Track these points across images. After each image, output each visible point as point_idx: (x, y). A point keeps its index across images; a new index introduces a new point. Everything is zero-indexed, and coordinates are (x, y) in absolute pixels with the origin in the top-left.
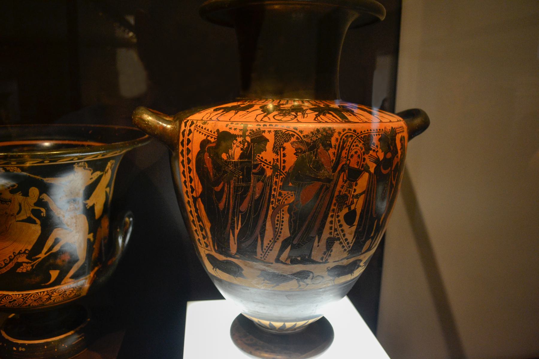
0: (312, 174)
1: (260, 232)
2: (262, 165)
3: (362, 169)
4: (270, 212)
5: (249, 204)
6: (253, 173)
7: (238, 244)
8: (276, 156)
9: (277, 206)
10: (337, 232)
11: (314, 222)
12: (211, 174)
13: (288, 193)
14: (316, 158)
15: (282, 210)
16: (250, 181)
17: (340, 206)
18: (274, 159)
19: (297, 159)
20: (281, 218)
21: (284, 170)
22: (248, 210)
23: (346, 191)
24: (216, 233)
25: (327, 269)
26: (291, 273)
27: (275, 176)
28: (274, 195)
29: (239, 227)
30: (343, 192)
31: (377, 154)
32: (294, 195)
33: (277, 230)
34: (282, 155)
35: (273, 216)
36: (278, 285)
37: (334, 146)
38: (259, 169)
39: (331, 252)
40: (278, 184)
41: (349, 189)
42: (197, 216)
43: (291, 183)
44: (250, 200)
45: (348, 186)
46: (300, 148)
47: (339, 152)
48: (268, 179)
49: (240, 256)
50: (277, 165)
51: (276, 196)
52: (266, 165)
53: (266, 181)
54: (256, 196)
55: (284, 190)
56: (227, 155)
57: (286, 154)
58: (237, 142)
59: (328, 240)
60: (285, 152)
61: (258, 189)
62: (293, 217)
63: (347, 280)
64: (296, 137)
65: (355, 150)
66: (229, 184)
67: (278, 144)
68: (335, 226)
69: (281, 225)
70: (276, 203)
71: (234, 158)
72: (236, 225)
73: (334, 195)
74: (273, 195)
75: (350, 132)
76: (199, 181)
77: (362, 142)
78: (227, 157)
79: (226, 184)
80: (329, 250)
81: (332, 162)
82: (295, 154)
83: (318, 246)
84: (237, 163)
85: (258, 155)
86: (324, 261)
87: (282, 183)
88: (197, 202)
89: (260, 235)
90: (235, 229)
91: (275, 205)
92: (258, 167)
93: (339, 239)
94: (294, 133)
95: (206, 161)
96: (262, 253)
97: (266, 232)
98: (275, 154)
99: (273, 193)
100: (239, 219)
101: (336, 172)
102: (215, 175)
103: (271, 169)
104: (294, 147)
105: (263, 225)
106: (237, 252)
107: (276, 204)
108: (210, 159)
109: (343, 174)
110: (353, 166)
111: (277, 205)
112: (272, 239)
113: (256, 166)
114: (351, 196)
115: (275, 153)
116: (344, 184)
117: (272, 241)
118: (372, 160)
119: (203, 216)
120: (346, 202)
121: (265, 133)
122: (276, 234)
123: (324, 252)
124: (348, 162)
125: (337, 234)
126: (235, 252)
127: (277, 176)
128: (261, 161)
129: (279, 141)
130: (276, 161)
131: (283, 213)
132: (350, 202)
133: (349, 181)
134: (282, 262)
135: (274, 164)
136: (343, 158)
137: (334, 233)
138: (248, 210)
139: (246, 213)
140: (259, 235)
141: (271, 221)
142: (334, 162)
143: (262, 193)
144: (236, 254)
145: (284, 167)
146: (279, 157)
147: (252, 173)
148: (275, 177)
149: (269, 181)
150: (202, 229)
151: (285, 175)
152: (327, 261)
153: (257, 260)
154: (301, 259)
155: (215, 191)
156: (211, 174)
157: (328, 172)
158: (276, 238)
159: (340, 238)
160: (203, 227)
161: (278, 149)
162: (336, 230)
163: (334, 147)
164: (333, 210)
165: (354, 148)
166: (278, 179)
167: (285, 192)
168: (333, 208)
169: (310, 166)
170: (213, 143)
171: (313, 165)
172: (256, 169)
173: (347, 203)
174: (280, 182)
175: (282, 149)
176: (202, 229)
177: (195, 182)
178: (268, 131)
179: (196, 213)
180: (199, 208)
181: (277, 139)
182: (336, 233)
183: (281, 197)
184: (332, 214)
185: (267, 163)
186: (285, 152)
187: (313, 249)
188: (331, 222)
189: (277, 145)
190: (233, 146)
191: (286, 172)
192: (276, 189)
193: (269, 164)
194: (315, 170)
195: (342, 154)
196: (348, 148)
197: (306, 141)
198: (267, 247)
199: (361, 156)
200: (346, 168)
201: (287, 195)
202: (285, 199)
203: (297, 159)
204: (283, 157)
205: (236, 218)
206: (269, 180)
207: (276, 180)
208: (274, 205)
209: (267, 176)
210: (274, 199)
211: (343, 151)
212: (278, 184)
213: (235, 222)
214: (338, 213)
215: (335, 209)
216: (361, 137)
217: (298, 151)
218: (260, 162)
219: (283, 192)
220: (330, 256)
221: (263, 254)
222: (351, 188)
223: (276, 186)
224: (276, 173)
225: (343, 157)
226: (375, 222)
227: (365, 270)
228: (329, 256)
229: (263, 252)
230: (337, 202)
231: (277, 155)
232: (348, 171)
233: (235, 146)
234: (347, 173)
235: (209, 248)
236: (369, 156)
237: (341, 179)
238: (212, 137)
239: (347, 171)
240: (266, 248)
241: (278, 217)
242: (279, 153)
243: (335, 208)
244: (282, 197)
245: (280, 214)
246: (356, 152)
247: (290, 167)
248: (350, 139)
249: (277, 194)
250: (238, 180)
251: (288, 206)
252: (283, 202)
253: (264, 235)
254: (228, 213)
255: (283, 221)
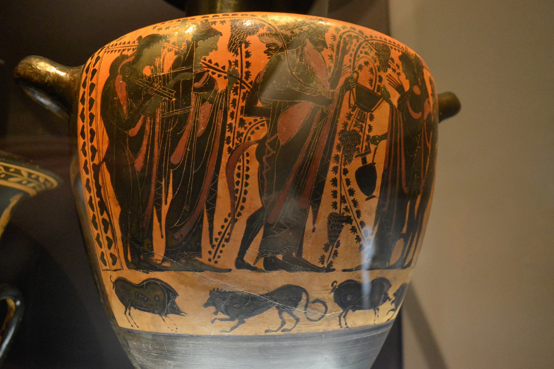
0: (295, 86)
1: (206, 202)
2: (209, 73)
3: (379, 94)
4: (224, 160)
5: (187, 147)
6: (195, 90)
7: (167, 240)
8: (233, 56)
9: (238, 146)
10: (346, 204)
11: (304, 179)
12: (125, 108)
13: (255, 120)
14: (301, 60)
15: (245, 153)
16: (189, 105)
17: (347, 151)
18: (230, 62)
19: (269, 60)
20: (245, 170)
21: (247, 80)
22: (184, 160)
23: (355, 126)
24: (129, 224)
25: (332, 285)
26: (266, 292)
27: (232, 91)
28: (231, 125)
29: (169, 201)
30: (351, 127)
31: (400, 78)
32: (266, 125)
33: (238, 195)
34: (244, 54)
35: (230, 167)
36: (244, 322)
37: (330, 46)
38: (206, 80)
39: (337, 247)
40: (237, 104)
41: (361, 123)
42: (99, 202)
43: (261, 102)
44: (189, 140)
45: (358, 118)
46: (275, 44)
47: (339, 57)
48: (220, 96)
49: (172, 263)
50: (235, 71)
51: (235, 127)
52: (218, 73)
53: (216, 101)
54: (200, 131)
55: (249, 115)
56: (152, 67)
57: (250, 52)
58: (170, 44)
59: (331, 218)
60: (249, 49)
61: (203, 117)
62: (267, 167)
63: (368, 324)
64: (267, 28)
65: (365, 60)
66: (153, 116)
67: (238, 38)
68: (341, 190)
69: (244, 184)
70: (236, 141)
71: (163, 69)
72: (164, 195)
73: (336, 129)
74: (228, 125)
75: (353, 32)
76: (105, 129)
77: (375, 51)
78: (152, 70)
79: (148, 118)
80: (334, 241)
81: (328, 71)
82: (265, 52)
83: (314, 230)
84: (168, 77)
85: (203, 57)
86: (326, 265)
87: (245, 101)
88: (100, 173)
89: (207, 209)
90: (161, 204)
91: (233, 145)
92: (203, 77)
93: (349, 220)
94: (263, 23)
95: (118, 90)
96: (211, 249)
97: (219, 201)
98: (233, 54)
99: (229, 121)
100: (168, 183)
101: (337, 88)
102: (130, 108)
103: (225, 78)
104: (265, 41)
105: (212, 187)
106: (165, 255)
107: (235, 142)
108: (125, 84)
109: (349, 94)
110: (362, 84)
111: (237, 144)
112: (229, 216)
113: (199, 76)
114: (365, 137)
115: (232, 52)
116: (352, 113)
117: (229, 219)
118: (393, 84)
119: (109, 197)
120: (357, 147)
121: (215, 24)
122: (236, 203)
123: (325, 245)
124: (355, 75)
125: (346, 209)
126: (163, 255)
127: (235, 90)
128: (209, 67)
129: (238, 34)
130: (234, 65)
131: (248, 158)
132: (364, 149)
133: (359, 109)
134: (249, 267)
135: (231, 70)
136: (346, 66)
137: (341, 206)
138: (184, 160)
139: (182, 166)
140: (205, 210)
141: (226, 178)
142: (332, 71)
143: (210, 125)
144: (164, 261)
145: (248, 74)
146: (238, 58)
147: (192, 89)
148: (233, 92)
149: (222, 101)
150: (107, 224)
151: (249, 87)
152: (332, 266)
153: (201, 268)
154: (283, 258)
155: (129, 136)
156: (125, 108)
157: (323, 86)
158: (237, 213)
159: (352, 218)
160: (108, 220)
161: (237, 46)
162: (343, 200)
163: (330, 48)
164: (337, 157)
165: (361, 55)
166: (237, 95)
167: (251, 119)
168: (336, 153)
169: (291, 72)
170: (131, 56)
171: (297, 71)
172: (200, 81)
173: (358, 148)
174: (241, 100)
175: (243, 45)
176: (107, 224)
177: (98, 137)
178: (220, 21)
179: (98, 197)
180: (103, 183)
181: (235, 30)
182: (343, 206)
183: (243, 128)
184: (335, 165)
185: (220, 68)
186: (249, 49)
187: (305, 238)
188: (334, 182)
189: (235, 40)
190: (163, 51)
191: (251, 83)
192: (235, 113)
193: (222, 70)
194: (301, 80)
195: (344, 61)
196: (353, 53)
197: (284, 33)
198: (220, 233)
199: (376, 82)
200: (353, 85)
201: (253, 123)
202: (250, 131)
203: (269, 60)
204: (246, 58)
205: (163, 181)
206: (223, 98)
207: (235, 98)
208: (231, 145)
209: (219, 91)
210: (231, 133)
211: (346, 56)
212: (237, 104)
213: (161, 188)
214: (344, 165)
215: (340, 156)
216: (372, 43)
217: (270, 48)
218: (206, 69)
219: (249, 119)
220: (337, 256)
221: (213, 252)
222: (363, 122)
223: (234, 108)
224: (235, 85)
225: (346, 65)
226: (407, 204)
227: (392, 327)
228: (334, 254)
229: (213, 246)
230: (342, 143)
231: (236, 55)
232: (356, 89)
233: (166, 50)
234: (355, 94)
235: (118, 266)
236: (387, 76)
237: (345, 103)
238: (129, 50)
239: (354, 90)
240: (217, 236)
241: (239, 168)
242: (239, 52)
243: (339, 153)
244: (245, 128)
245: (242, 161)
246: (367, 63)
247: (259, 74)
248: (355, 41)
249: (235, 123)
250: (169, 106)
251: (257, 144)
252: (247, 138)
253: (215, 208)
254: (150, 177)
255: (247, 177)
